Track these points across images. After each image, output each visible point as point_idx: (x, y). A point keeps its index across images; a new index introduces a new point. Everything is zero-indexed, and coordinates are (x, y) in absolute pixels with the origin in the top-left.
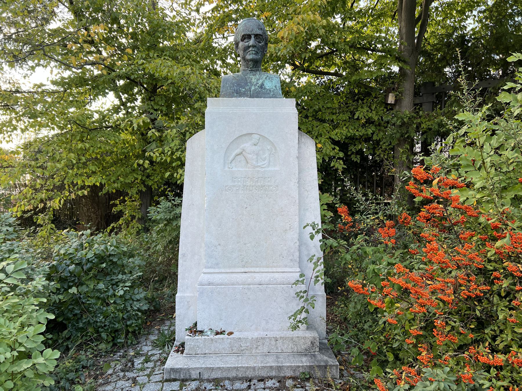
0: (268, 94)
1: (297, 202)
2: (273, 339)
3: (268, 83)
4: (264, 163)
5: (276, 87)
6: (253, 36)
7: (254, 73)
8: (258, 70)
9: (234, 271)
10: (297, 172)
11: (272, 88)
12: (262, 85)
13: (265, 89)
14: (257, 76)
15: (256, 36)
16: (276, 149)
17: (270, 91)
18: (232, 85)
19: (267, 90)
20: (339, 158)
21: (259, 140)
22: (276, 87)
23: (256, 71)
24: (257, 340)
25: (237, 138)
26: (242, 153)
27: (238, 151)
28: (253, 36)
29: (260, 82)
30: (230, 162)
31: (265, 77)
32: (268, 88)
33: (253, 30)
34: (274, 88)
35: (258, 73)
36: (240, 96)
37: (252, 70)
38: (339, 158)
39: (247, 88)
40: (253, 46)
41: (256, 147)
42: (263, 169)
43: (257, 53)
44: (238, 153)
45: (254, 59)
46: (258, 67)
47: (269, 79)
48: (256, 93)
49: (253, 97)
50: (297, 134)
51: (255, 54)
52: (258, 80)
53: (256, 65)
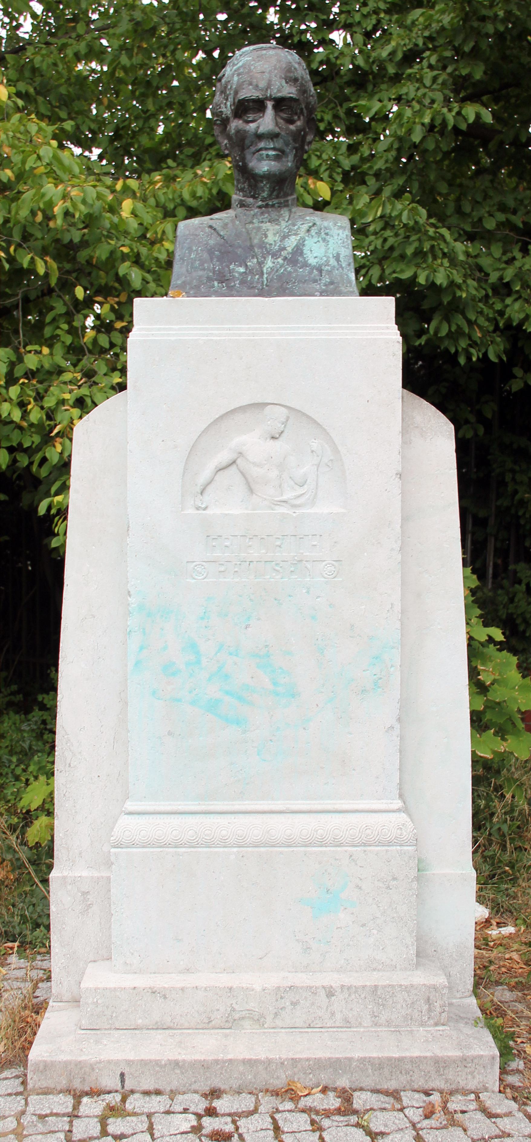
0: (315, 281)
1: (398, 608)
2: (322, 993)
3: (315, 247)
4: (301, 491)
5: (337, 258)
6: (270, 105)
7: (274, 214)
8: (286, 205)
9: (211, 808)
10: (398, 519)
11: (327, 264)
12: (298, 250)
13: (306, 264)
14: (283, 224)
15: (280, 104)
16: (336, 450)
17: (320, 271)
18: (206, 255)
19: (313, 268)
20: (419, 1122)
21: (285, 423)
22: (337, 258)
23: (281, 206)
24: (280, 992)
25: (222, 417)
26: (234, 462)
27: (224, 457)
28: (270, 105)
29: (291, 243)
30: (199, 489)
31: (305, 227)
32: (312, 261)
33: (269, 86)
34: (333, 262)
35: (285, 212)
36: (231, 292)
37: (267, 206)
38: (419, 1122)
39: (252, 263)
40: (273, 136)
41: (277, 443)
42: (299, 511)
43: (281, 155)
44: (224, 464)
45: (275, 175)
46: (286, 195)
47: (318, 233)
48: (280, 277)
49: (269, 295)
50: (398, 404)
51: (277, 158)
52: (284, 237)
53: (281, 189)
